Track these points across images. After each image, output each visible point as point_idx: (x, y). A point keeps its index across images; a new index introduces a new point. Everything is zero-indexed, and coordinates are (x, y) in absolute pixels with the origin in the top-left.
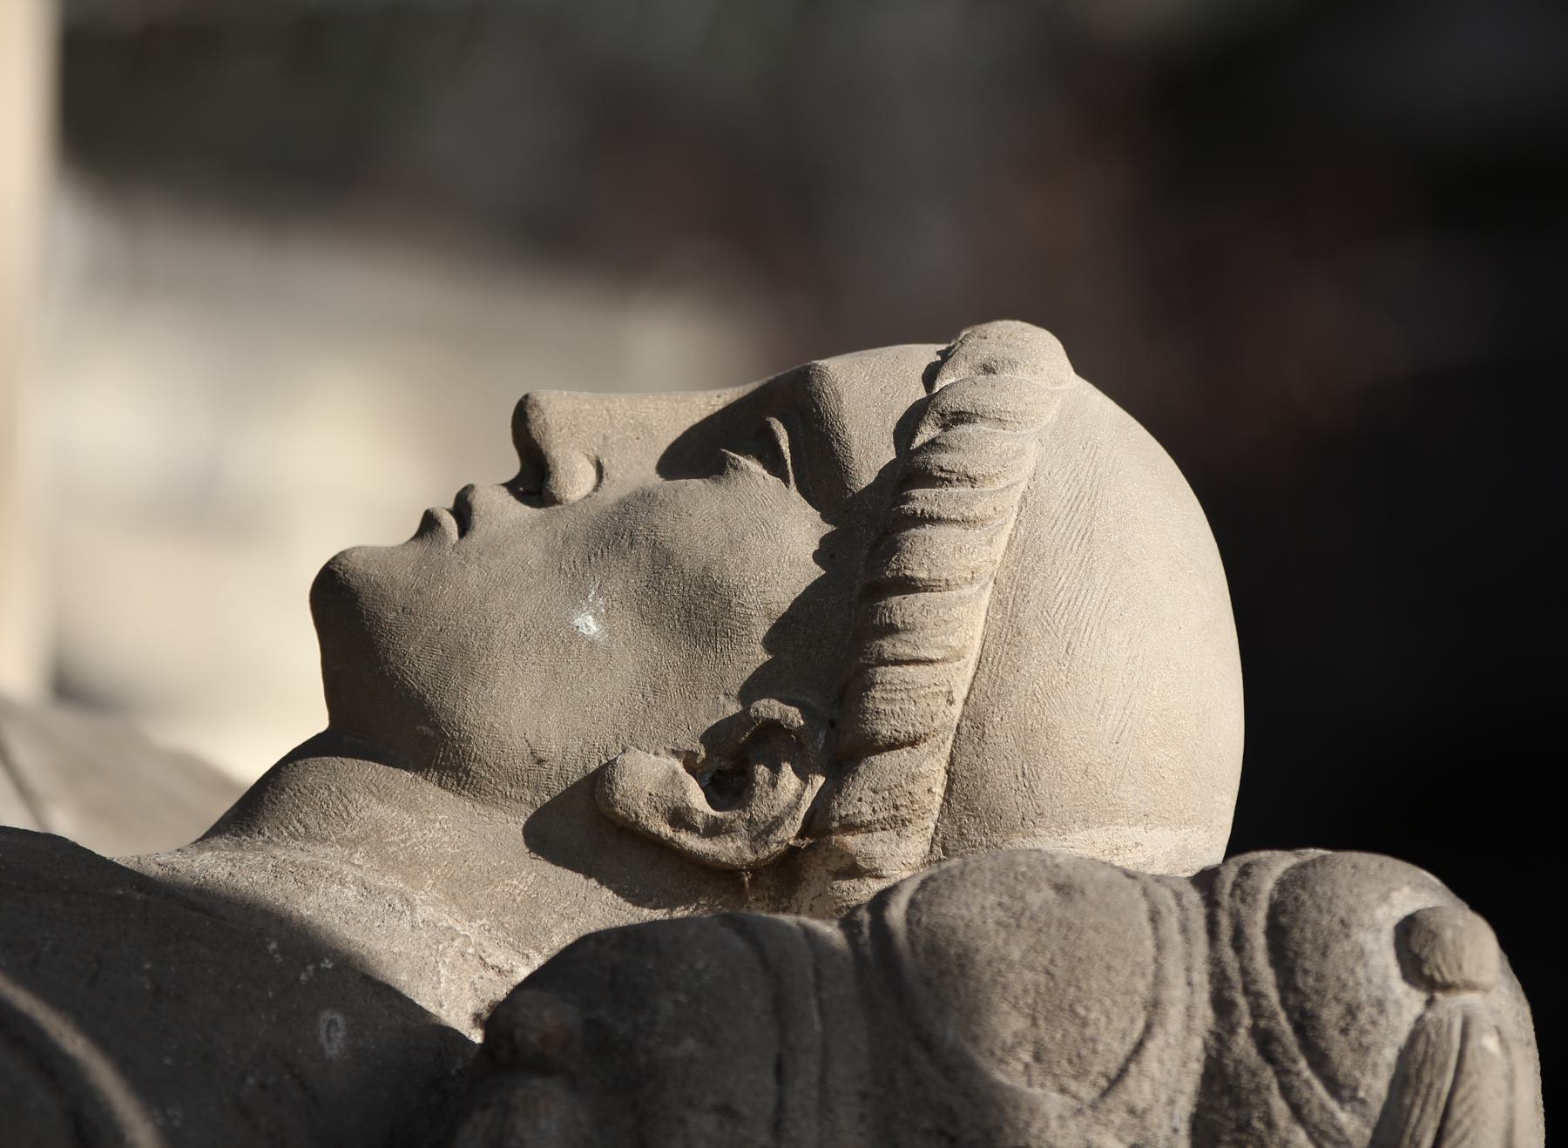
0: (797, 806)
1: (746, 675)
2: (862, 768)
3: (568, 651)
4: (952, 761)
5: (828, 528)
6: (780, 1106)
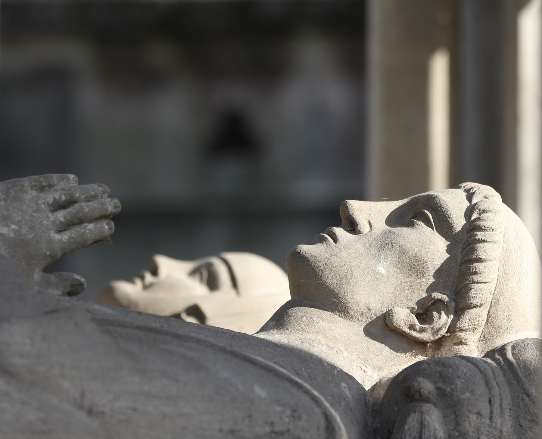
0: (446, 324)
1: (428, 285)
2: (466, 313)
3: (376, 278)
4: (489, 312)
5: (448, 243)
6: (491, 412)
